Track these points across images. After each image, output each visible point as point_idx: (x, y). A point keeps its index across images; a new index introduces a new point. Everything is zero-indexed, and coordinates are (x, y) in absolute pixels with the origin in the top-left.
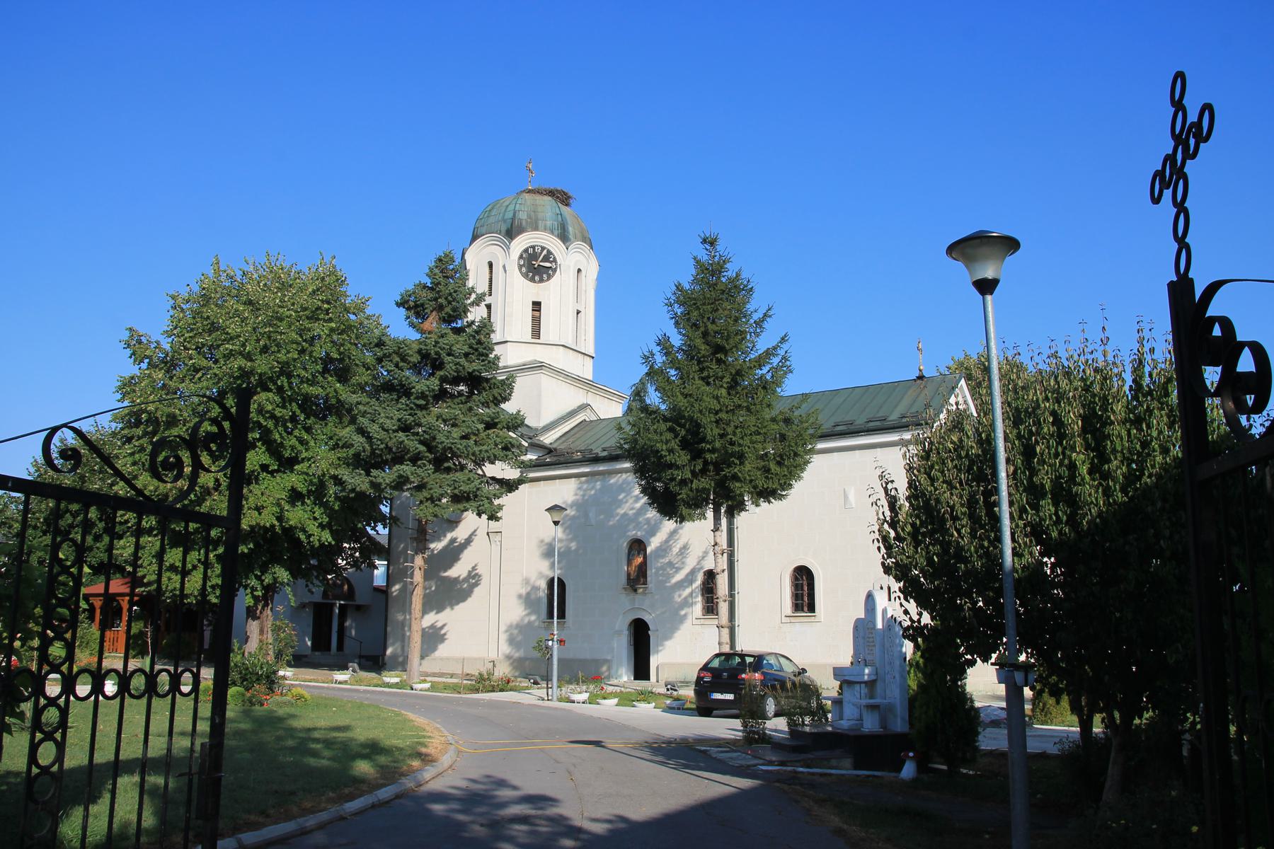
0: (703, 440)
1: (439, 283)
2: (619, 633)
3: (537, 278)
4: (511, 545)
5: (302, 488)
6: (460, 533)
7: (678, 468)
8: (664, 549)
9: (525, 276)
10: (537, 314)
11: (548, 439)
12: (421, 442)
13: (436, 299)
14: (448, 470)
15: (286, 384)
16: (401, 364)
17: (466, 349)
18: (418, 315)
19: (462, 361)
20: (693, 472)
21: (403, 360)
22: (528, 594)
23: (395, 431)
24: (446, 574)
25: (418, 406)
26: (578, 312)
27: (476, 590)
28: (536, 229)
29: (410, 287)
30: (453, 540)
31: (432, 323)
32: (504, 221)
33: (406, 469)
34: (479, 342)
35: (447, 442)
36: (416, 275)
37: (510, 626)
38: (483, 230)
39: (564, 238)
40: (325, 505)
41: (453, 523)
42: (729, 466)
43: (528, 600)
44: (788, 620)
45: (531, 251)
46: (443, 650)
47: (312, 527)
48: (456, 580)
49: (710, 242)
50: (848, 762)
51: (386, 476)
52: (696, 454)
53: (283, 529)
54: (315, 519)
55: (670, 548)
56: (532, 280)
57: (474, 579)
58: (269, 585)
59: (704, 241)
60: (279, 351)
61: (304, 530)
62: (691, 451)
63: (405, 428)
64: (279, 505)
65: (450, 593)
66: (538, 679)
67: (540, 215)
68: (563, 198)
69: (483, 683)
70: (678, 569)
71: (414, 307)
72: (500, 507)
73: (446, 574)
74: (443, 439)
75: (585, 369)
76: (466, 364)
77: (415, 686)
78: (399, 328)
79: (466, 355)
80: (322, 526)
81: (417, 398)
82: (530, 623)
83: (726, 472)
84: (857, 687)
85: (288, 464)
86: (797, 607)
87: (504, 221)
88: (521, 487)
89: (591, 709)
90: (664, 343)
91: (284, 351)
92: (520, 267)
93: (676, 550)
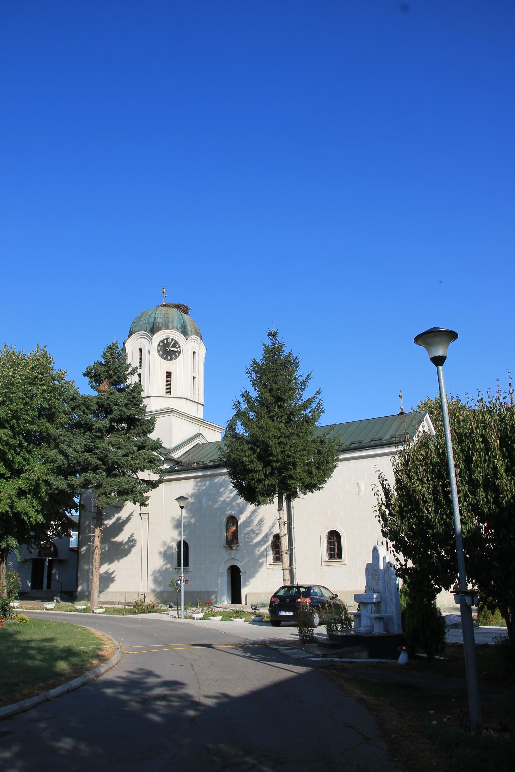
0: (271, 455)
1: (109, 362)
2: (222, 574)
3: (169, 358)
4: (154, 521)
5: (25, 488)
6: (123, 514)
7: (256, 472)
9: (162, 356)
10: (169, 379)
11: (176, 455)
12: (99, 459)
13: (107, 371)
14: (115, 476)
15: (16, 424)
16: (86, 411)
17: (126, 401)
18: (96, 381)
19: (124, 409)
20: (265, 475)
21: (88, 408)
22: (165, 551)
23: (82, 452)
24: (115, 540)
25: (96, 436)
26: (194, 378)
28: (168, 328)
29: (92, 364)
30: (119, 519)
31: (105, 386)
32: (149, 323)
33: (89, 475)
34: (134, 397)
35: (114, 459)
36: (95, 356)
37: (155, 572)
38: (136, 329)
39: (185, 333)
40: (40, 499)
41: (119, 508)
42: (287, 470)
43: (166, 555)
44: (326, 564)
45: (165, 341)
46: (113, 587)
47: (32, 512)
48: (121, 543)
49: (273, 335)
50: (365, 654)
51: (77, 480)
52: (267, 464)
53: (14, 513)
54: (33, 507)
56: (166, 359)
57: (132, 542)
58: (4, 548)
59: (269, 334)
60: (11, 404)
61: (26, 514)
62: (264, 462)
63: (89, 450)
64: (11, 498)
65: (117, 552)
66: (172, 605)
67: (170, 320)
68: (184, 309)
69: (138, 608)
70: (257, 534)
71: (94, 376)
72: (148, 498)
73: (115, 540)
74: (112, 457)
75: (199, 412)
76: (126, 411)
77: (95, 611)
78: (85, 389)
79: (126, 405)
80: (37, 511)
81: (96, 432)
82: (166, 569)
83: (285, 474)
84: (369, 606)
85: (17, 473)
86: (331, 556)
87: (149, 323)
88: (160, 485)
89: (205, 623)
91: (14, 404)
92: (159, 351)
93: (256, 522)
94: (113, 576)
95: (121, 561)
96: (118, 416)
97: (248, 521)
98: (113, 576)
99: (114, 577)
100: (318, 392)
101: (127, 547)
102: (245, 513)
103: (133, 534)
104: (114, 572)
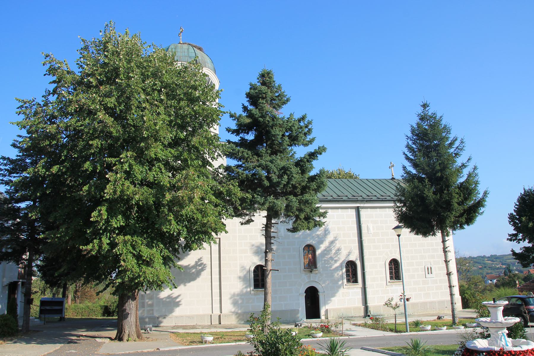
8: (327, 250)
27: (203, 273)
43: (244, 279)
46: (178, 311)
48: (187, 267)
55: (331, 250)
70: (336, 261)
82: (247, 292)
90: (408, 146)
93: (333, 251)
94: (178, 300)
95: (188, 285)
96: (465, 172)
97: (328, 249)
98: (178, 300)
99: (180, 301)
100: (469, 159)
101: (194, 271)
102: (324, 243)
103: (201, 258)
104: (179, 296)
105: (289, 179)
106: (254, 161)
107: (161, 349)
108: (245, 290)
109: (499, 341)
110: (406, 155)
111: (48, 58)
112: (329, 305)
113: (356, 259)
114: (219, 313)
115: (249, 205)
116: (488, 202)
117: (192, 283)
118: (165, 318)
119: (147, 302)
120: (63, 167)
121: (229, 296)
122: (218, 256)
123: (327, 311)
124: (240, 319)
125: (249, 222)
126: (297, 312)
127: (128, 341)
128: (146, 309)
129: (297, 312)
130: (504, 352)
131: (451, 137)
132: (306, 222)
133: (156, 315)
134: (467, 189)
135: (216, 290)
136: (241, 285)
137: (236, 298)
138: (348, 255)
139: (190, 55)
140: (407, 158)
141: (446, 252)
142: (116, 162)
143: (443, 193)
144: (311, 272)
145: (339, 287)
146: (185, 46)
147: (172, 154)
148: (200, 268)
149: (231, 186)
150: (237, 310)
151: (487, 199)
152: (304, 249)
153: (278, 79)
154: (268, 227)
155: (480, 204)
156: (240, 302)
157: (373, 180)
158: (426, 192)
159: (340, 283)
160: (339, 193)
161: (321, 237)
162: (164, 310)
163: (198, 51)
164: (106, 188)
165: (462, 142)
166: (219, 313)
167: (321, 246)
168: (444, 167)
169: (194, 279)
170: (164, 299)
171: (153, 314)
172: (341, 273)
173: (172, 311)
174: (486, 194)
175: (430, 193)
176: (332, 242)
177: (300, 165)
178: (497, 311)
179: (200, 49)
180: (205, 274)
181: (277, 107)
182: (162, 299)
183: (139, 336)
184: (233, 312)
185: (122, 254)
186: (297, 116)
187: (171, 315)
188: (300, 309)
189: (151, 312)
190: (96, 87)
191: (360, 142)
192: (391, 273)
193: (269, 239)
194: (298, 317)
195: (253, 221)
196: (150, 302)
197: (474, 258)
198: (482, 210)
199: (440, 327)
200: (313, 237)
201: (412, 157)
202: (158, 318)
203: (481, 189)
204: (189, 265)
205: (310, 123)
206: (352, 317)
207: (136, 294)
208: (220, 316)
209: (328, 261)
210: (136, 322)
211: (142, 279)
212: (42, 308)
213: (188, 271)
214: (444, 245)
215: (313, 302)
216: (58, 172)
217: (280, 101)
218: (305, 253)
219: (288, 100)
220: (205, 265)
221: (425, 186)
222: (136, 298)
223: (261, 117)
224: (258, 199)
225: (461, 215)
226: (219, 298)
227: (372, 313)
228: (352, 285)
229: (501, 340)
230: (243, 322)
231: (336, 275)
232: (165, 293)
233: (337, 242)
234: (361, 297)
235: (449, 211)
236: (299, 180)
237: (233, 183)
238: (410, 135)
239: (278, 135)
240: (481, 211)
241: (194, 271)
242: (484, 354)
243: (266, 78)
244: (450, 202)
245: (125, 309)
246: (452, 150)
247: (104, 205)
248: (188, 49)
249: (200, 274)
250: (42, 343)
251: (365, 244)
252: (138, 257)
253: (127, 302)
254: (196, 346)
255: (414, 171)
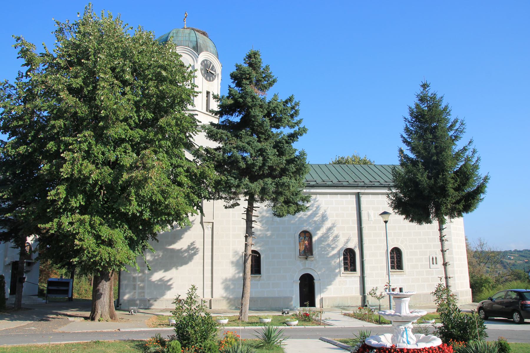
8: (325, 237)
27: (195, 257)
28: (207, 51)
43: (235, 264)
45: (205, 62)
48: (179, 251)
55: (328, 237)
70: (333, 249)
90: (407, 130)
94: (169, 283)
97: (325, 236)
98: (169, 283)
99: (171, 285)
100: (470, 142)
101: (186, 254)
102: (321, 229)
103: (194, 242)
104: (171, 279)
105: (265, 160)
106: (235, 142)
107: (122, 330)
108: (237, 276)
109: (400, 337)
110: (404, 138)
111: (19, 41)
112: (325, 293)
113: (355, 247)
114: (210, 298)
115: (223, 188)
116: (489, 188)
117: (184, 267)
118: (156, 301)
119: (139, 285)
120: (31, 147)
121: (221, 281)
122: (211, 240)
123: (322, 300)
124: (232, 305)
125: (233, 206)
126: (290, 299)
127: (99, 321)
128: (137, 291)
129: (291, 299)
130: (395, 350)
131: (452, 118)
132: (286, 206)
133: (147, 297)
134: (464, 175)
135: (208, 275)
136: (234, 270)
137: (228, 283)
138: (347, 242)
139: (191, 39)
140: (405, 141)
141: (443, 240)
142: (73, 141)
143: (438, 177)
144: (306, 258)
145: (336, 275)
146: (188, 31)
147: (139, 134)
148: (193, 252)
149: (207, 168)
150: (228, 296)
151: (487, 185)
152: (300, 235)
153: (264, 61)
154: (249, 211)
155: (480, 190)
156: (232, 287)
157: (381, 166)
158: (419, 176)
159: (337, 271)
160: (341, 179)
161: (318, 223)
162: (155, 293)
163: (199, 35)
164: (62, 167)
165: (462, 124)
166: (210, 298)
167: (318, 232)
168: (441, 150)
169: (186, 263)
170: (156, 282)
171: (144, 296)
172: (338, 261)
173: (163, 294)
174: (486, 179)
175: (423, 178)
176: (330, 229)
177: (279, 146)
178: (401, 302)
179: (204, 34)
180: (197, 259)
181: (263, 88)
182: (154, 282)
183: (112, 316)
184: (224, 298)
185: (79, 233)
186: (283, 98)
187: (162, 298)
188: (294, 297)
189: (142, 294)
190: (66, 68)
191: (350, 124)
192: (392, 262)
193: (249, 223)
194: (292, 305)
195: (238, 205)
196: (141, 285)
197: (520, 251)
198: (482, 196)
199: (428, 320)
200: (310, 223)
201: (409, 140)
202: (149, 301)
203: (482, 172)
204: (182, 249)
205: (297, 104)
206: (348, 306)
207: (110, 275)
208: (210, 301)
209: (325, 248)
210: (110, 302)
211: (97, 258)
212: (50, 288)
213: (180, 254)
214: (441, 233)
215: (308, 289)
216: (26, 152)
217: (265, 81)
218: (301, 239)
219: (274, 81)
220: (198, 249)
221: (418, 170)
222: (110, 279)
223: (240, 98)
224: (232, 181)
225: (458, 202)
226: (210, 283)
227: (370, 303)
228: (349, 274)
229: (402, 336)
230: (234, 308)
231: (333, 262)
232: (156, 277)
233: (335, 229)
234: (359, 286)
235: (444, 197)
236: (276, 162)
237: (209, 165)
238: (409, 118)
239: (258, 116)
240: (481, 198)
241: (186, 254)
242: (375, 351)
243: (252, 60)
244: (445, 187)
245: (99, 290)
246: (451, 133)
247: (64, 185)
248: (189, 34)
249: (192, 259)
250: (12, 320)
251: (365, 232)
252: (97, 237)
253: (100, 282)
254: (161, 329)
255: (412, 156)
